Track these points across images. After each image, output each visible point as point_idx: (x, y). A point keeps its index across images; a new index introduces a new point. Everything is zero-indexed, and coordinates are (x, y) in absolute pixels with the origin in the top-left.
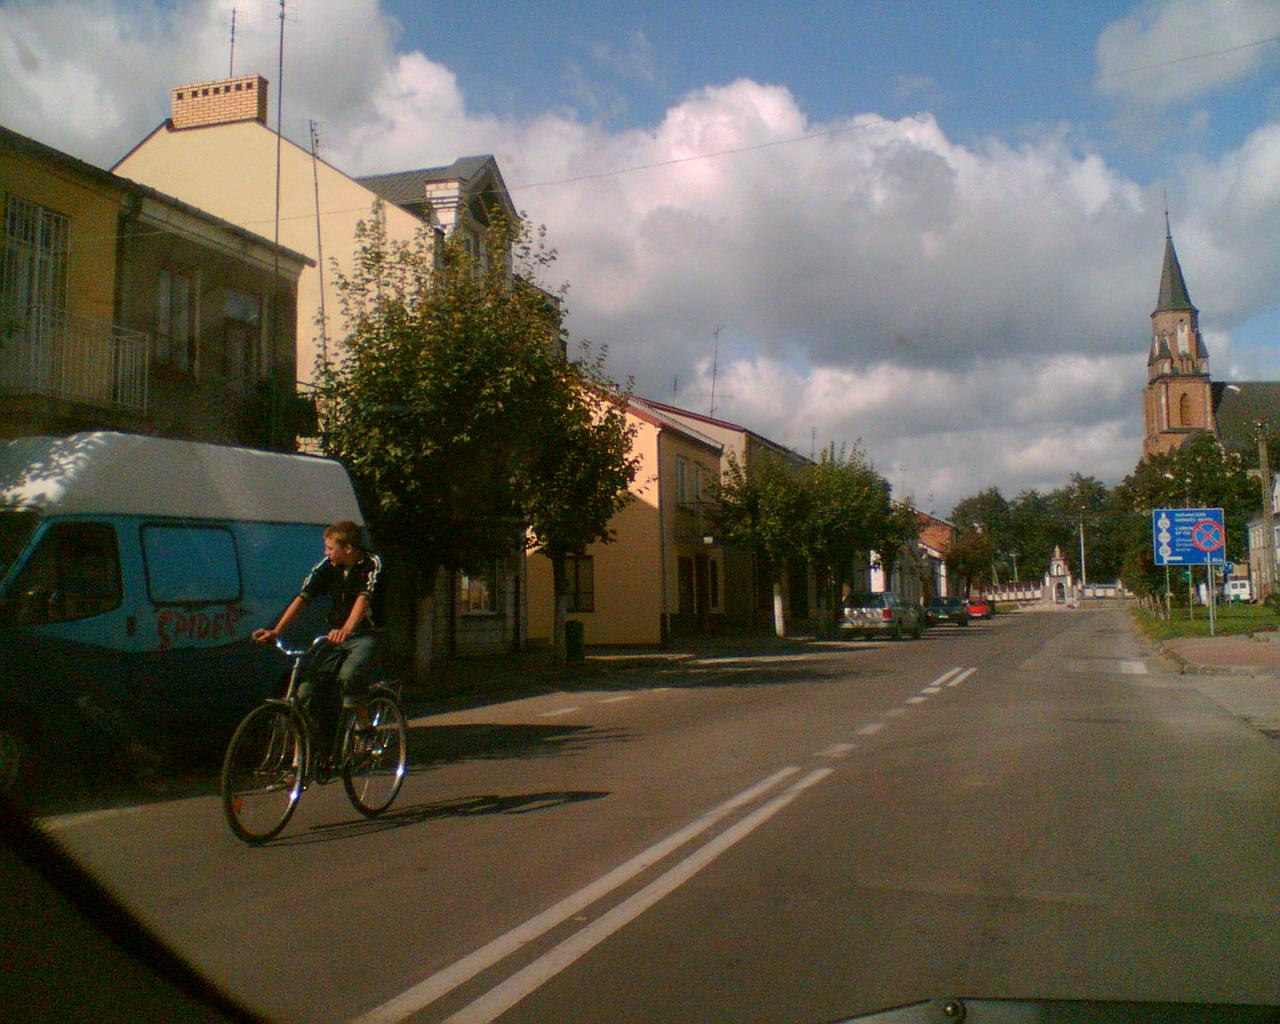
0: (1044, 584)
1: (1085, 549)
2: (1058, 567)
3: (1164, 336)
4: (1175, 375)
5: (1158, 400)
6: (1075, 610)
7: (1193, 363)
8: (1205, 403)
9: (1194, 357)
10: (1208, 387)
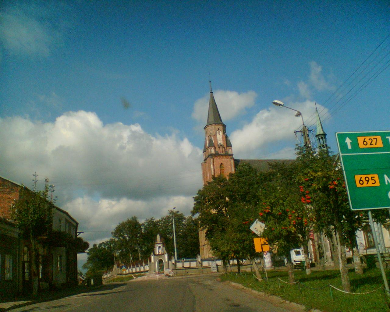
0: (150, 261)
1: (177, 245)
2: (159, 249)
3: (211, 136)
4: (216, 155)
5: (210, 166)
6: (171, 278)
7: (225, 149)
8: (232, 168)
9: (225, 146)
10: (232, 161)
